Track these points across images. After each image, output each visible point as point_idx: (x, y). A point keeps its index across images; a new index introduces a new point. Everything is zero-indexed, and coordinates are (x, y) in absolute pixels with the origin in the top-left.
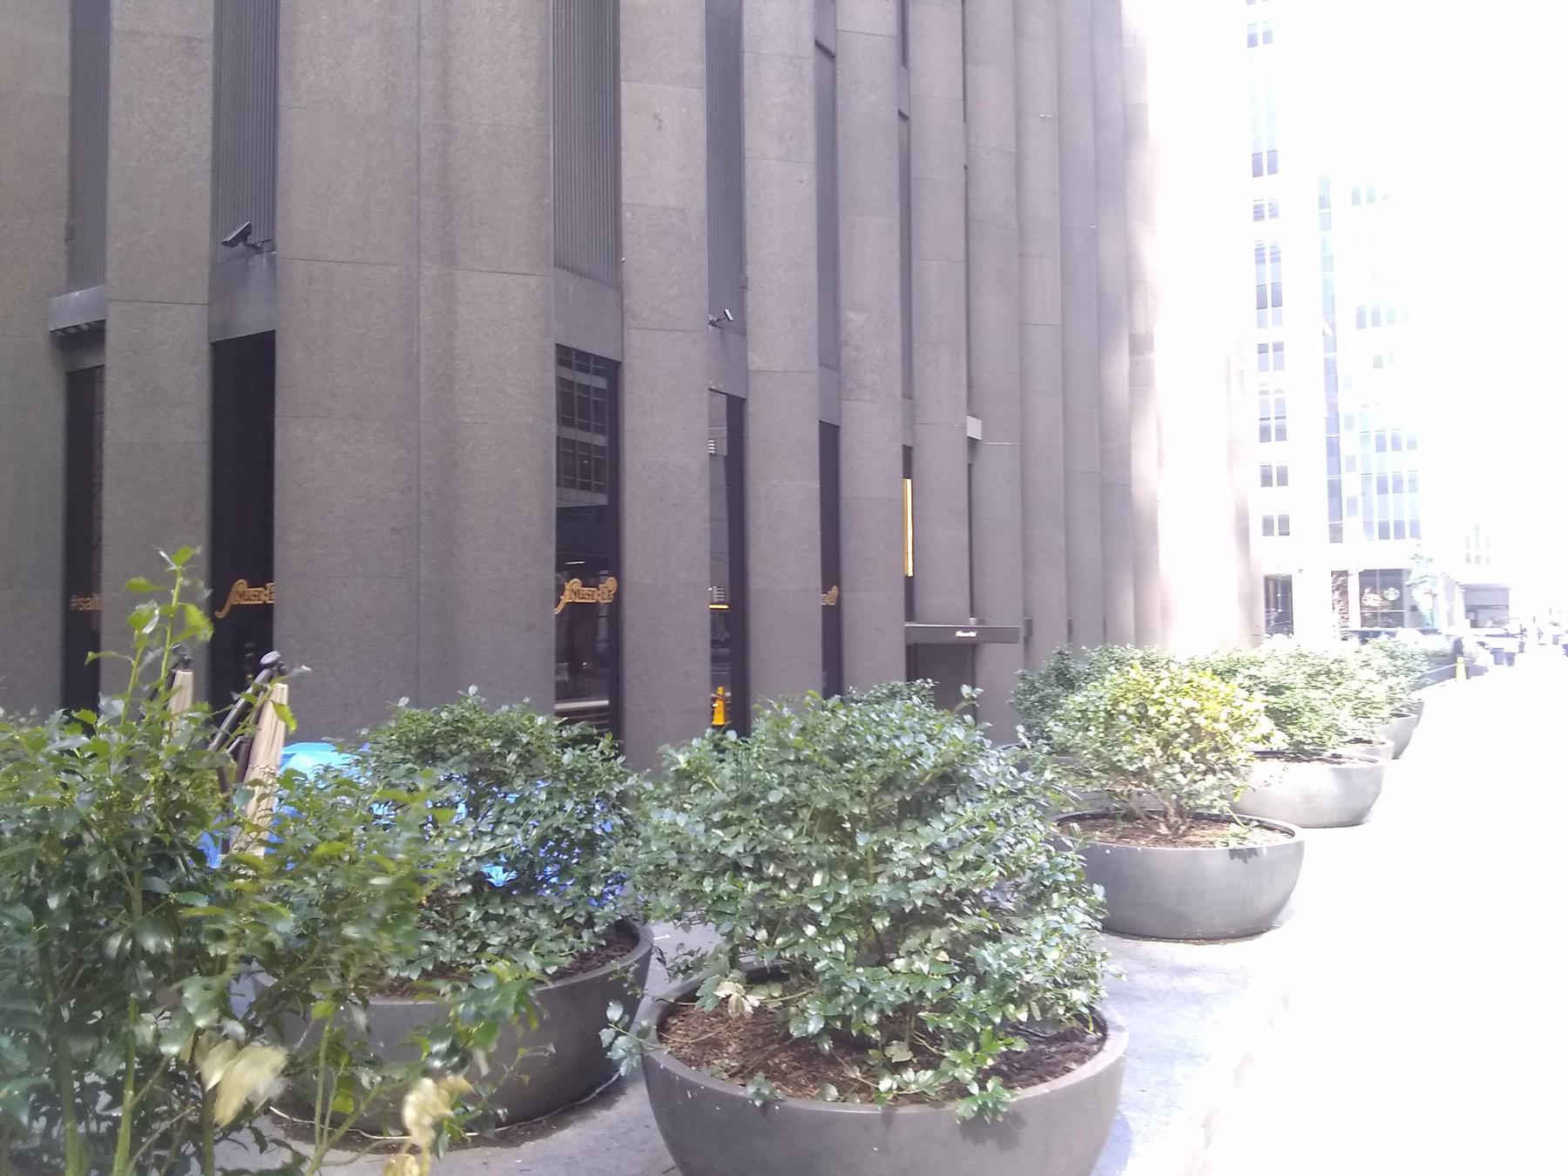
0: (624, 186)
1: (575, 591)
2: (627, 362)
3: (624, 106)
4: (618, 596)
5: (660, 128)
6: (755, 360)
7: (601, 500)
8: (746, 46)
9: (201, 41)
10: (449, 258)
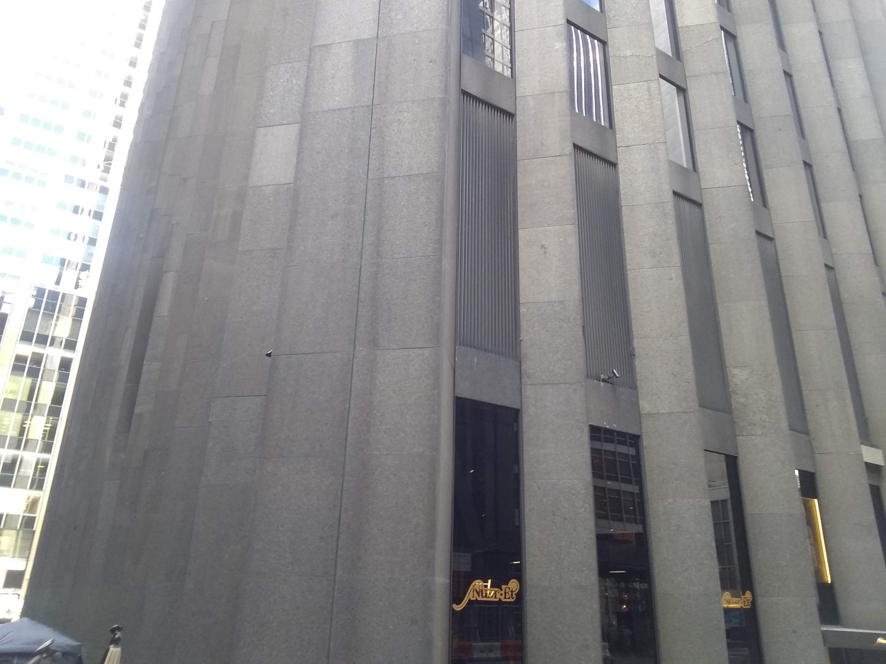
0: (521, 292)
1: (483, 589)
2: (644, 436)
3: (521, 243)
4: (520, 595)
5: (545, 253)
6: (645, 406)
7: (633, 529)
8: (623, 203)
9: (281, 249)
10: (374, 344)
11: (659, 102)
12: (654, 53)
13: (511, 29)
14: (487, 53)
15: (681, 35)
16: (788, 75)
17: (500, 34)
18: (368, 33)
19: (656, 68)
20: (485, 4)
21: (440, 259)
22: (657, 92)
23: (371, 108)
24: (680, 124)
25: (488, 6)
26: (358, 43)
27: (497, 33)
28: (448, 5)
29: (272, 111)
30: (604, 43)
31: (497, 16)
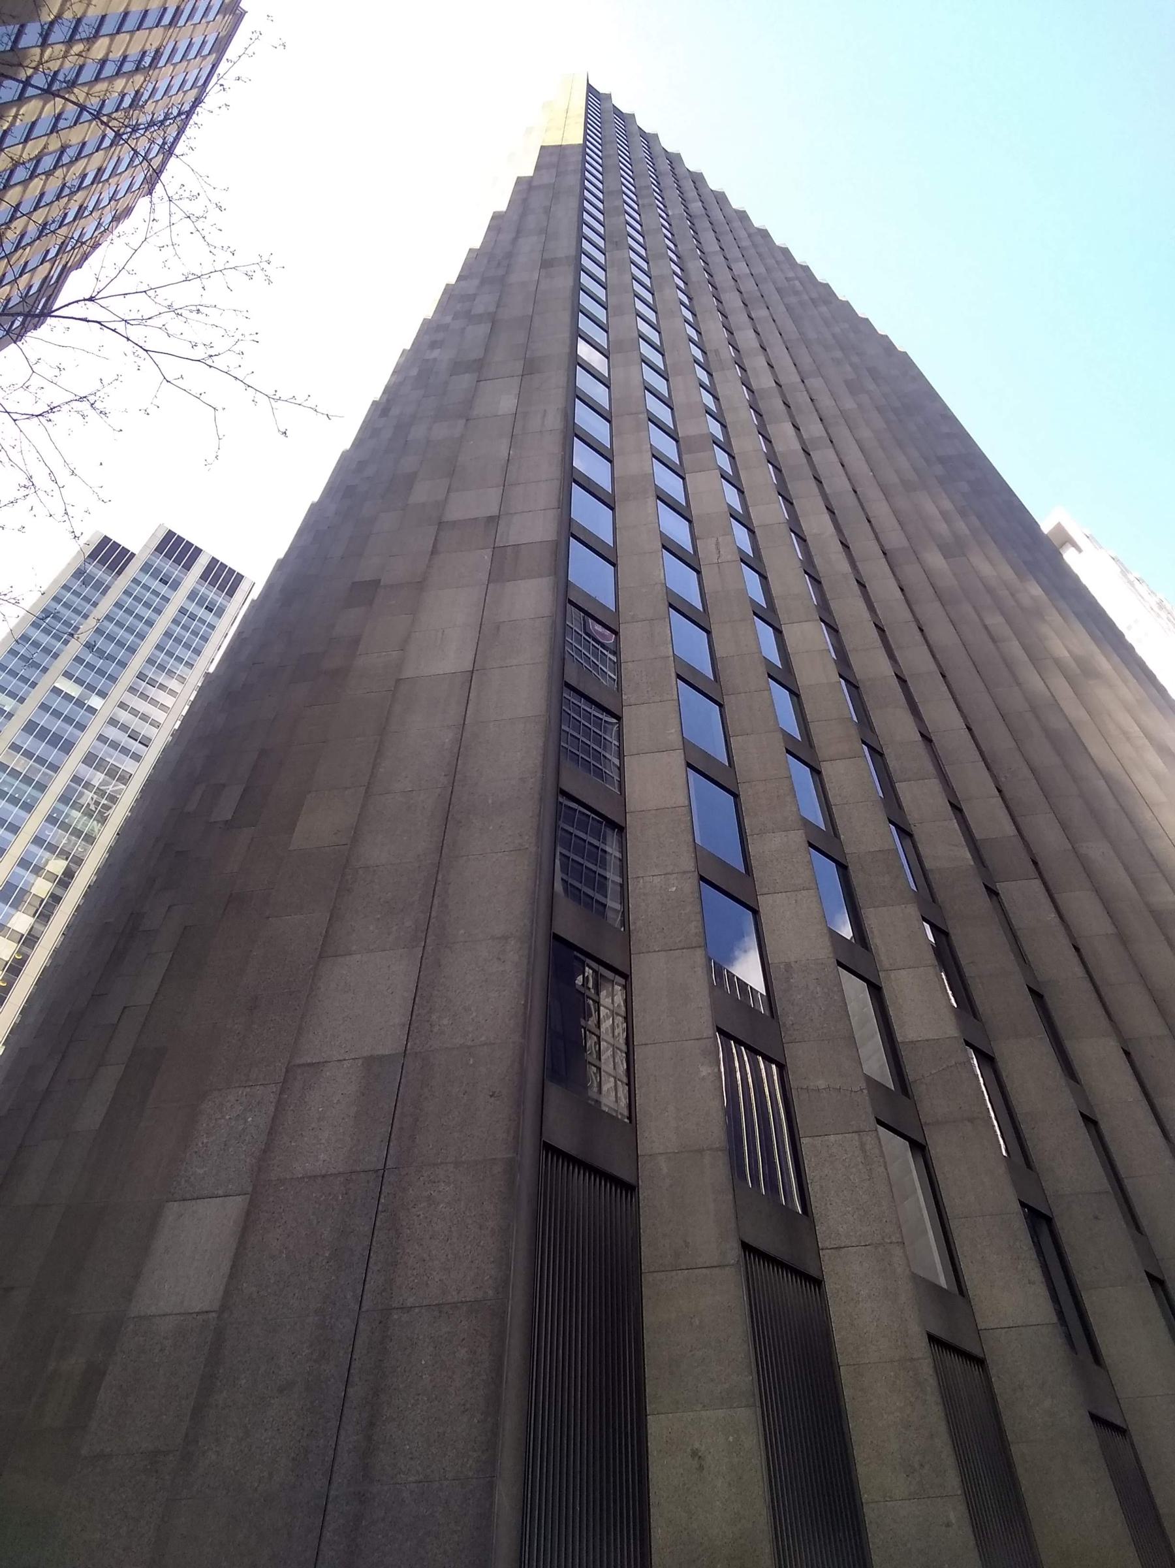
3: (652, 1445)
5: (701, 1468)
11: (882, 1169)
12: (864, 1085)
13: (628, 1018)
14: (589, 1059)
15: (904, 1053)
16: (1090, 1121)
17: (611, 1062)
18: (389, 1045)
19: (869, 1110)
20: (586, 980)
21: (490, 1487)
22: (877, 1151)
23: (381, 1174)
24: (919, 1191)
25: (590, 985)
26: (371, 1061)
27: (606, 1025)
28: (525, 1006)
29: (200, 1171)
30: (755, 912)
31: (605, 999)
